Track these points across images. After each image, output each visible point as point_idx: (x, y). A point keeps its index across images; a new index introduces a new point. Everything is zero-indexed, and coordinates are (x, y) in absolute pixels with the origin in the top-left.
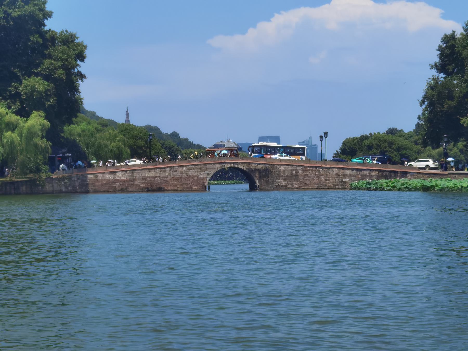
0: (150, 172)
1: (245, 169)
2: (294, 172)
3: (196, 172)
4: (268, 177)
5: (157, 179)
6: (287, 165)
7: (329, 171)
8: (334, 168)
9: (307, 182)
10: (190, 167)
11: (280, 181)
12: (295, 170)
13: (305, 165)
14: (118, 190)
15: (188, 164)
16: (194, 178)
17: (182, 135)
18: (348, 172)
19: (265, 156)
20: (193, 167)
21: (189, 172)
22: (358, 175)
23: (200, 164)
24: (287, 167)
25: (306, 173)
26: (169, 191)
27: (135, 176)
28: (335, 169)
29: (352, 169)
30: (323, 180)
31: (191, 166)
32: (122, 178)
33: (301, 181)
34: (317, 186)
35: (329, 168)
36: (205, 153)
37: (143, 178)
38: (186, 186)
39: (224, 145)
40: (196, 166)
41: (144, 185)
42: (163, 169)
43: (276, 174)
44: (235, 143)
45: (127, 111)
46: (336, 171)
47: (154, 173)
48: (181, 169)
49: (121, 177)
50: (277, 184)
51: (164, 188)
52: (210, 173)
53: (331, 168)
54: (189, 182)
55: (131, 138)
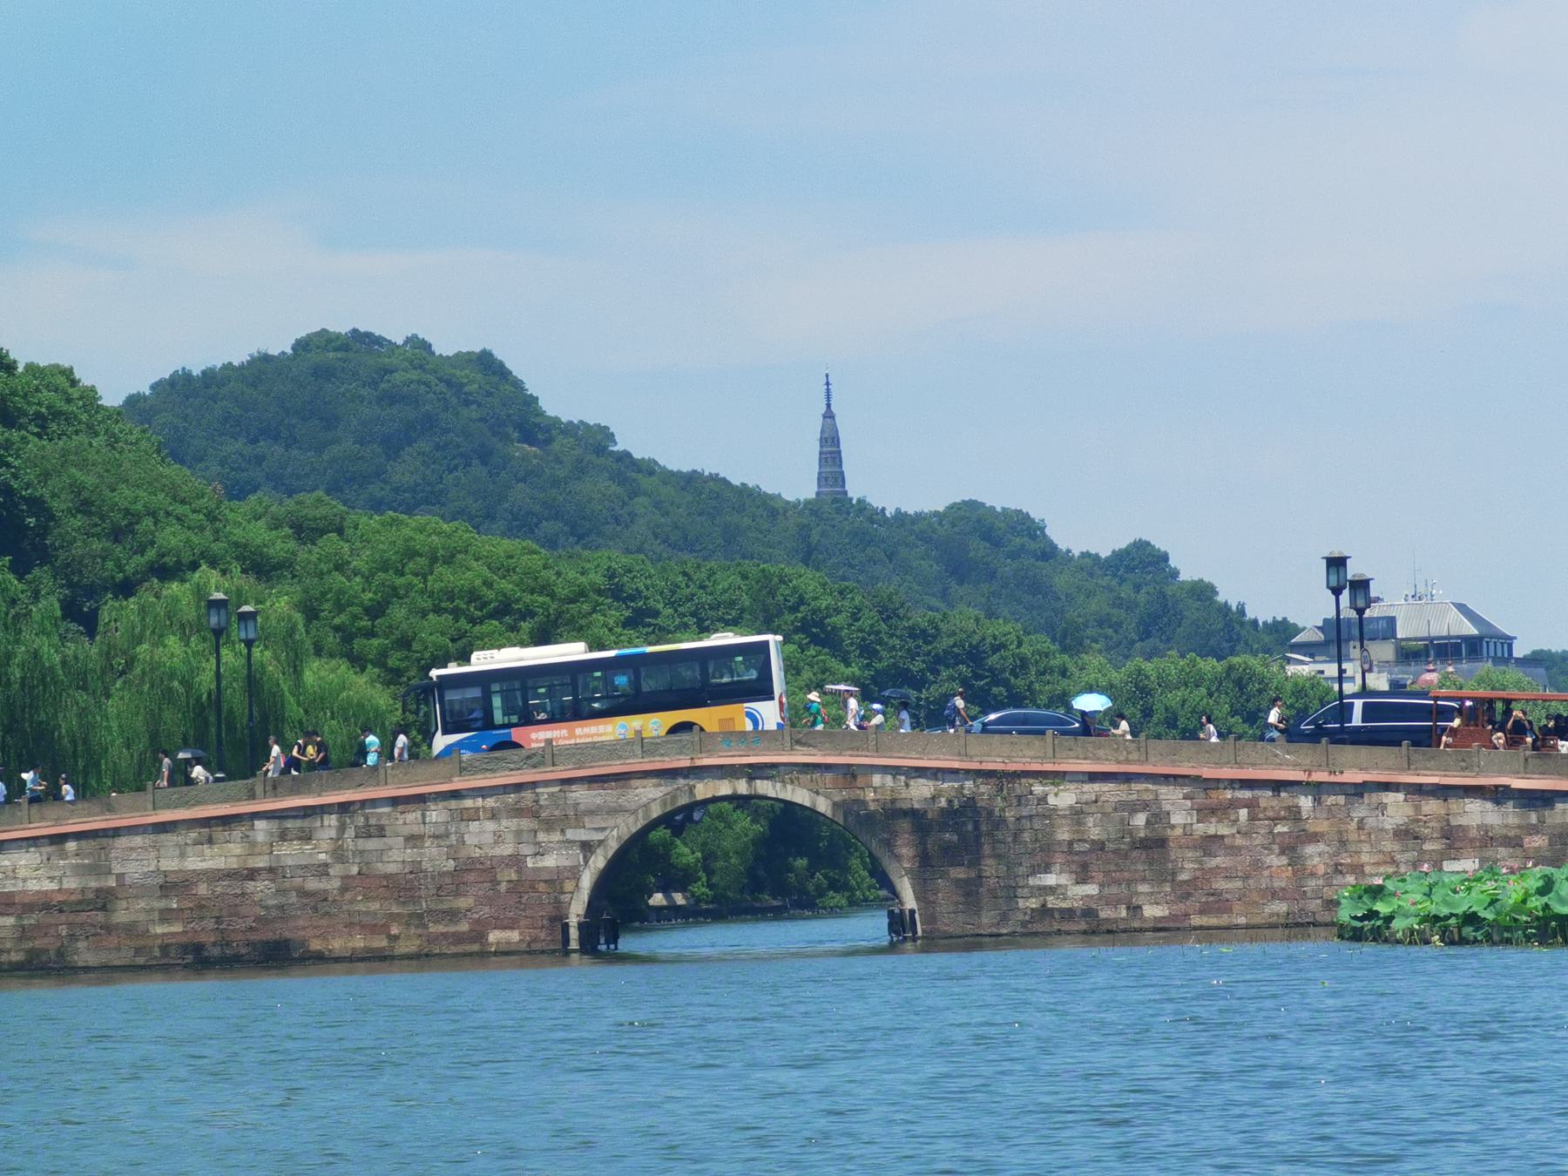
0: (210, 841)
1: (823, 806)
2: (1140, 820)
3: (509, 837)
4: (976, 862)
5: (261, 888)
6: (1094, 777)
7: (1359, 812)
8: (1387, 787)
9: (1221, 884)
10: (468, 803)
11: (1050, 879)
12: (1145, 806)
13: (1207, 772)
14: (10, 963)
15: (458, 784)
16: (499, 877)
17: (1189, 566)
18: (1475, 813)
19: (516, 734)
20: (491, 802)
21: (466, 837)
22: (1534, 830)
23: (534, 785)
24: (1096, 787)
25: (1212, 828)
26: (337, 960)
27: (117, 868)
28: (1391, 798)
29: (1498, 795)
30: (1321, 870)
31: (474, 797)
32: (33, 886)
33: (1184, 877)
34: (1281, 907)
35: (1358, 791)
36: (1229, 685)
37: (171, 885)
38: (441, 928)
39: (1392, 621)
40: (511, 798)
41: (177, 928)
42: (298, 823)
43: (1026, 836)
44: (1462, 608)
45: (829, 415)
46: (1397, 808)
47: (236, 848)
48: (413, 816)
49: (25, 880)
50: (1033, 903)
51: (303, 943)
52: (601, 842)
53: (1371, 792)
54: (463, 903)
55: (438, 610)
